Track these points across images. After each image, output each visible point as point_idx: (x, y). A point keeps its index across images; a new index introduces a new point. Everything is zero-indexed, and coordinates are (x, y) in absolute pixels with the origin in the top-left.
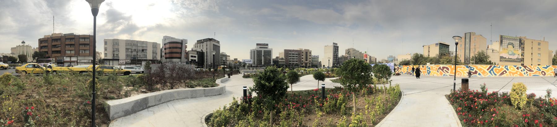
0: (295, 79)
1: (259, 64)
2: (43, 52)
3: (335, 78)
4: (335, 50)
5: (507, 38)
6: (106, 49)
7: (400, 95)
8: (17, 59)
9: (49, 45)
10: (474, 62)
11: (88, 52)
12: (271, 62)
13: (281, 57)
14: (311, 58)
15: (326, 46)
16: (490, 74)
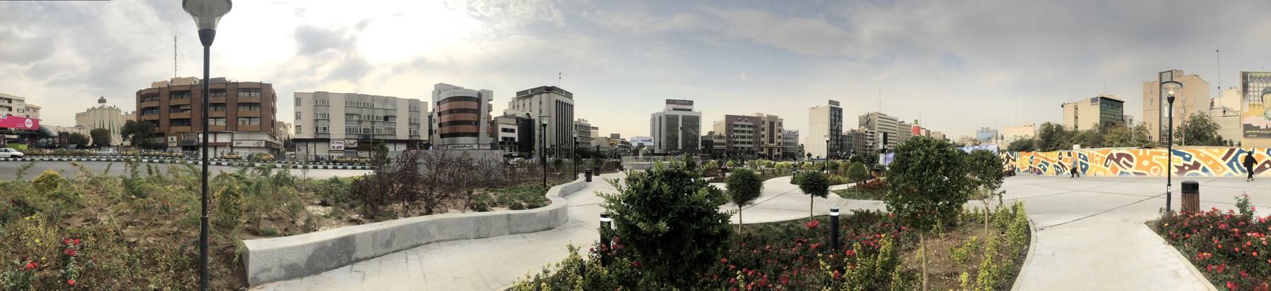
0: (747, 190)
1: (670, 149)
2: (148, 121)
4: (833, 118)
5: (1260, 77)
6: (298, 116)
7: (1026, 233)
8: (88, 140)
9: (162, 105)
10: (1183, 140)
11: (256, 123)
12: (698, 144)
13: (717, 133)
16: (1229, 170)
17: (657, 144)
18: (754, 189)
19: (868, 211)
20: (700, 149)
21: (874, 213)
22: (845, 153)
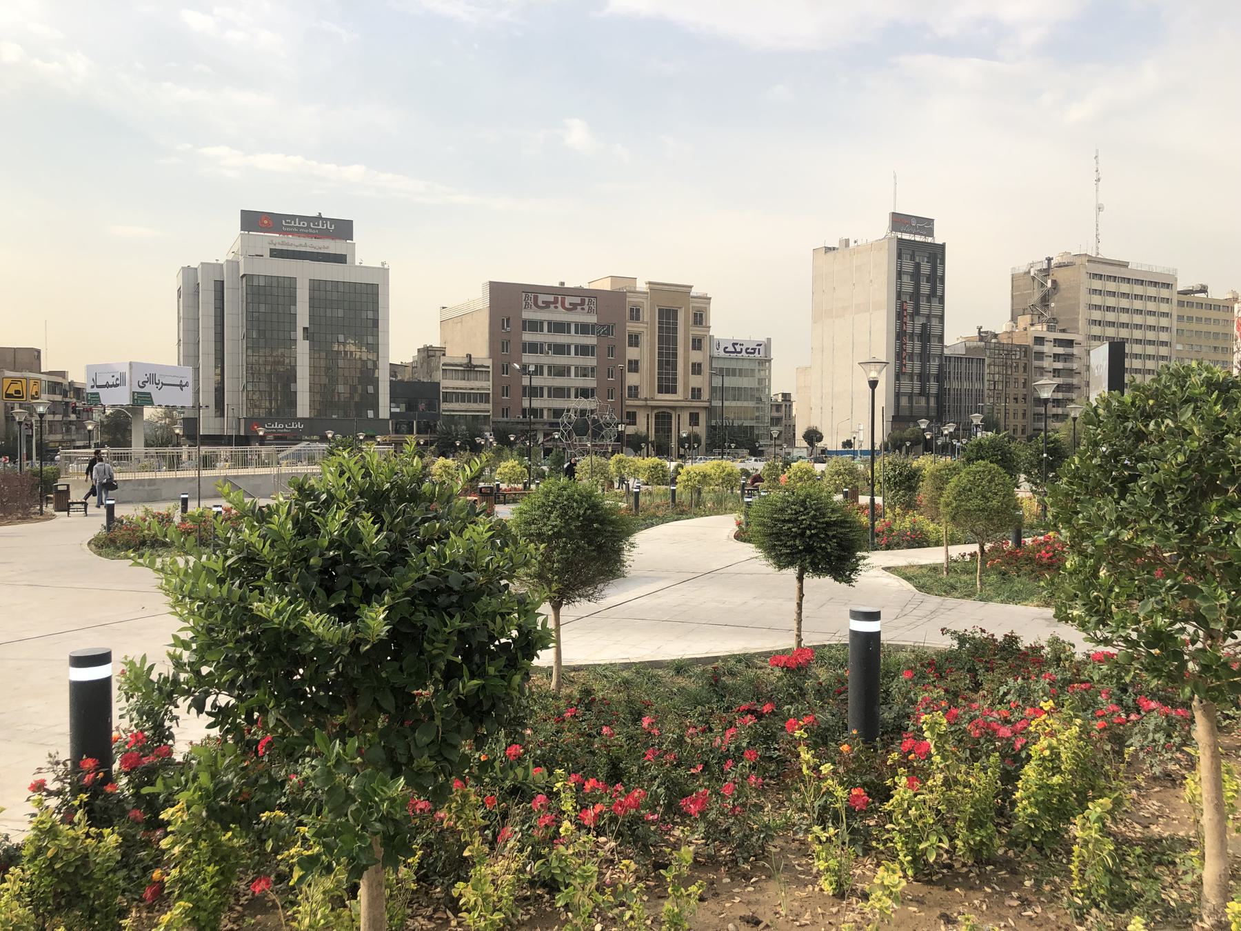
3: (932, 556)
4: (908, 288)
13: (456, 354)
14: (706, 369)
15: (828, 249)
17: (207, 398)
18: (600, 548)
19: (1011, 640)
20: (384, 413)
21: (1036, 649)
22: (949, 429)
